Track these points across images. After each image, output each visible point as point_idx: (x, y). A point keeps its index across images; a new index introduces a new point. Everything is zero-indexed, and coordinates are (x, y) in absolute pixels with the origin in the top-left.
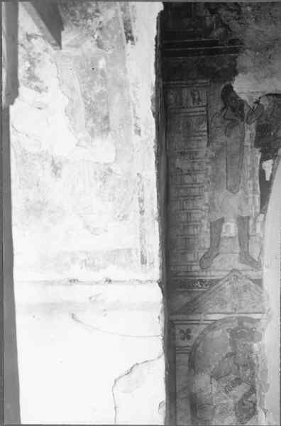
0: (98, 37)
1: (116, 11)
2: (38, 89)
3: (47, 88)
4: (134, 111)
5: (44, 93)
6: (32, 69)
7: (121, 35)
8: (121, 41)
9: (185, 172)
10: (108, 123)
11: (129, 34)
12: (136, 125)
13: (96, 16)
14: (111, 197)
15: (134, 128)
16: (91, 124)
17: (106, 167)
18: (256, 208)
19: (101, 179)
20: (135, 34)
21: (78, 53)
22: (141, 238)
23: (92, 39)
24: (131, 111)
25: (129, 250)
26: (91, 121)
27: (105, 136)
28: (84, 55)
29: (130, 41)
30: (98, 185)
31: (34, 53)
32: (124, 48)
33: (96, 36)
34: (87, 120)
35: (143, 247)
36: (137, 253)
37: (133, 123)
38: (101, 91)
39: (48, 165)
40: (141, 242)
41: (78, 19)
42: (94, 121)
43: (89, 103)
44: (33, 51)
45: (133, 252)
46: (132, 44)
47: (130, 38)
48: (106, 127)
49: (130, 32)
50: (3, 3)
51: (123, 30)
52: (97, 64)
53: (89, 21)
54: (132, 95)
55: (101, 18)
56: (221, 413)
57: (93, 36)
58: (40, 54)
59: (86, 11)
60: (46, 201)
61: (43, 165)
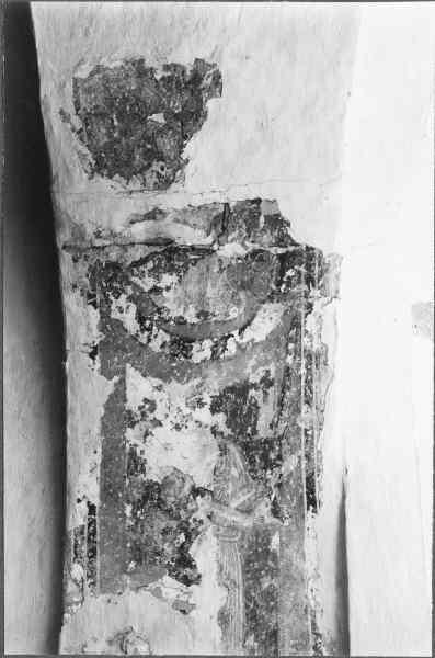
0: (275, 498)
1: (300, 457)
2: (187, 581)
3: (199, 576)
4: (314, 624)
5: (193, 586)
7: (302, 497)
9: (220, 439)
10: (276, 641)
13: (278, 466)
18: (89, 329)
20: (318, 495)
23: (267, 499)
24: (310, 623)
26: (252, 638)
31: (195, 520)
37: (312, 643)
41: (257, 468)
42: (257, 637)
47: (312, 502)
49: (313, 492)
51: (305, 490)
53: (269, 472)
56: (243, 210)
58: (201, 522)
59: (267, 456)
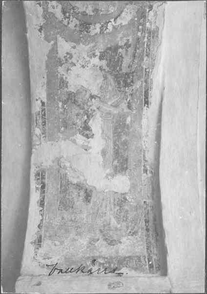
1: (142, 82)
4: (144, 156)
6: (87, 121)
7: (142, 100)
8: (141, 104)
11: (146, 100)
12: (144, 166)
14: (125, 219)
15: (143, 168)
16: (116, 162)
17: (123, 196)
19: (118, 205)
21: (115, 111)
22: (148, 249)
24: (142, 156)
25: (139, 258)
27: (124, 172)
28: (106, 103)
29: (146, 105)
30: (116, 210)
31: (91, 110)
32: (142, 109)
33: (128, 100)
34: (114, 160)
35: (149, 255)
36: (145, 259)
37: (143, 164)
38: (126, 139)
39: (82, 193)
40: (147, 251)
43: (117, 148)
44: (91, 108)
45: (142, 259)
46: (147, 107)
48: (125, 166)
50: (3, 2)
52: (125, 120)
54: (143, 144)
55: (134, 87)
57: (127, 100)
60: (76, 220)
61: (79, 193)
